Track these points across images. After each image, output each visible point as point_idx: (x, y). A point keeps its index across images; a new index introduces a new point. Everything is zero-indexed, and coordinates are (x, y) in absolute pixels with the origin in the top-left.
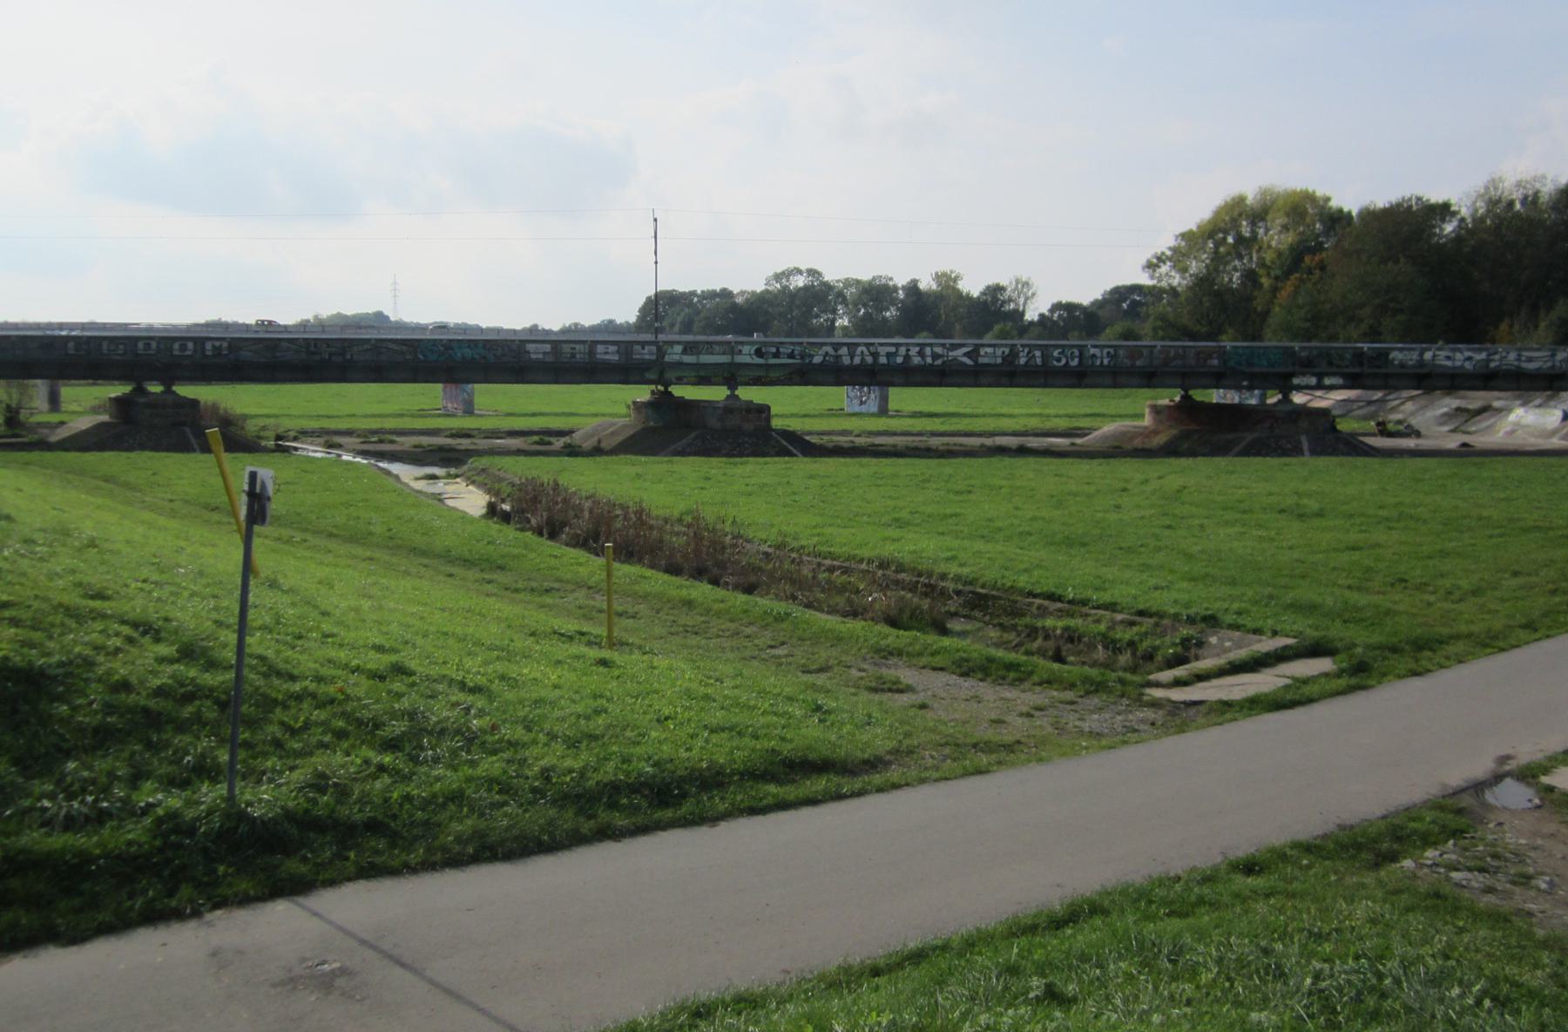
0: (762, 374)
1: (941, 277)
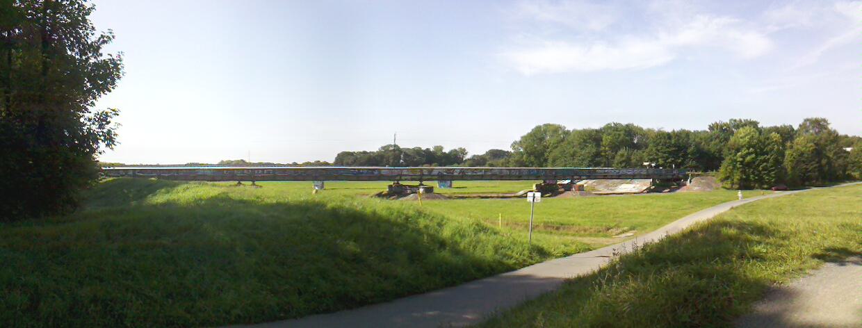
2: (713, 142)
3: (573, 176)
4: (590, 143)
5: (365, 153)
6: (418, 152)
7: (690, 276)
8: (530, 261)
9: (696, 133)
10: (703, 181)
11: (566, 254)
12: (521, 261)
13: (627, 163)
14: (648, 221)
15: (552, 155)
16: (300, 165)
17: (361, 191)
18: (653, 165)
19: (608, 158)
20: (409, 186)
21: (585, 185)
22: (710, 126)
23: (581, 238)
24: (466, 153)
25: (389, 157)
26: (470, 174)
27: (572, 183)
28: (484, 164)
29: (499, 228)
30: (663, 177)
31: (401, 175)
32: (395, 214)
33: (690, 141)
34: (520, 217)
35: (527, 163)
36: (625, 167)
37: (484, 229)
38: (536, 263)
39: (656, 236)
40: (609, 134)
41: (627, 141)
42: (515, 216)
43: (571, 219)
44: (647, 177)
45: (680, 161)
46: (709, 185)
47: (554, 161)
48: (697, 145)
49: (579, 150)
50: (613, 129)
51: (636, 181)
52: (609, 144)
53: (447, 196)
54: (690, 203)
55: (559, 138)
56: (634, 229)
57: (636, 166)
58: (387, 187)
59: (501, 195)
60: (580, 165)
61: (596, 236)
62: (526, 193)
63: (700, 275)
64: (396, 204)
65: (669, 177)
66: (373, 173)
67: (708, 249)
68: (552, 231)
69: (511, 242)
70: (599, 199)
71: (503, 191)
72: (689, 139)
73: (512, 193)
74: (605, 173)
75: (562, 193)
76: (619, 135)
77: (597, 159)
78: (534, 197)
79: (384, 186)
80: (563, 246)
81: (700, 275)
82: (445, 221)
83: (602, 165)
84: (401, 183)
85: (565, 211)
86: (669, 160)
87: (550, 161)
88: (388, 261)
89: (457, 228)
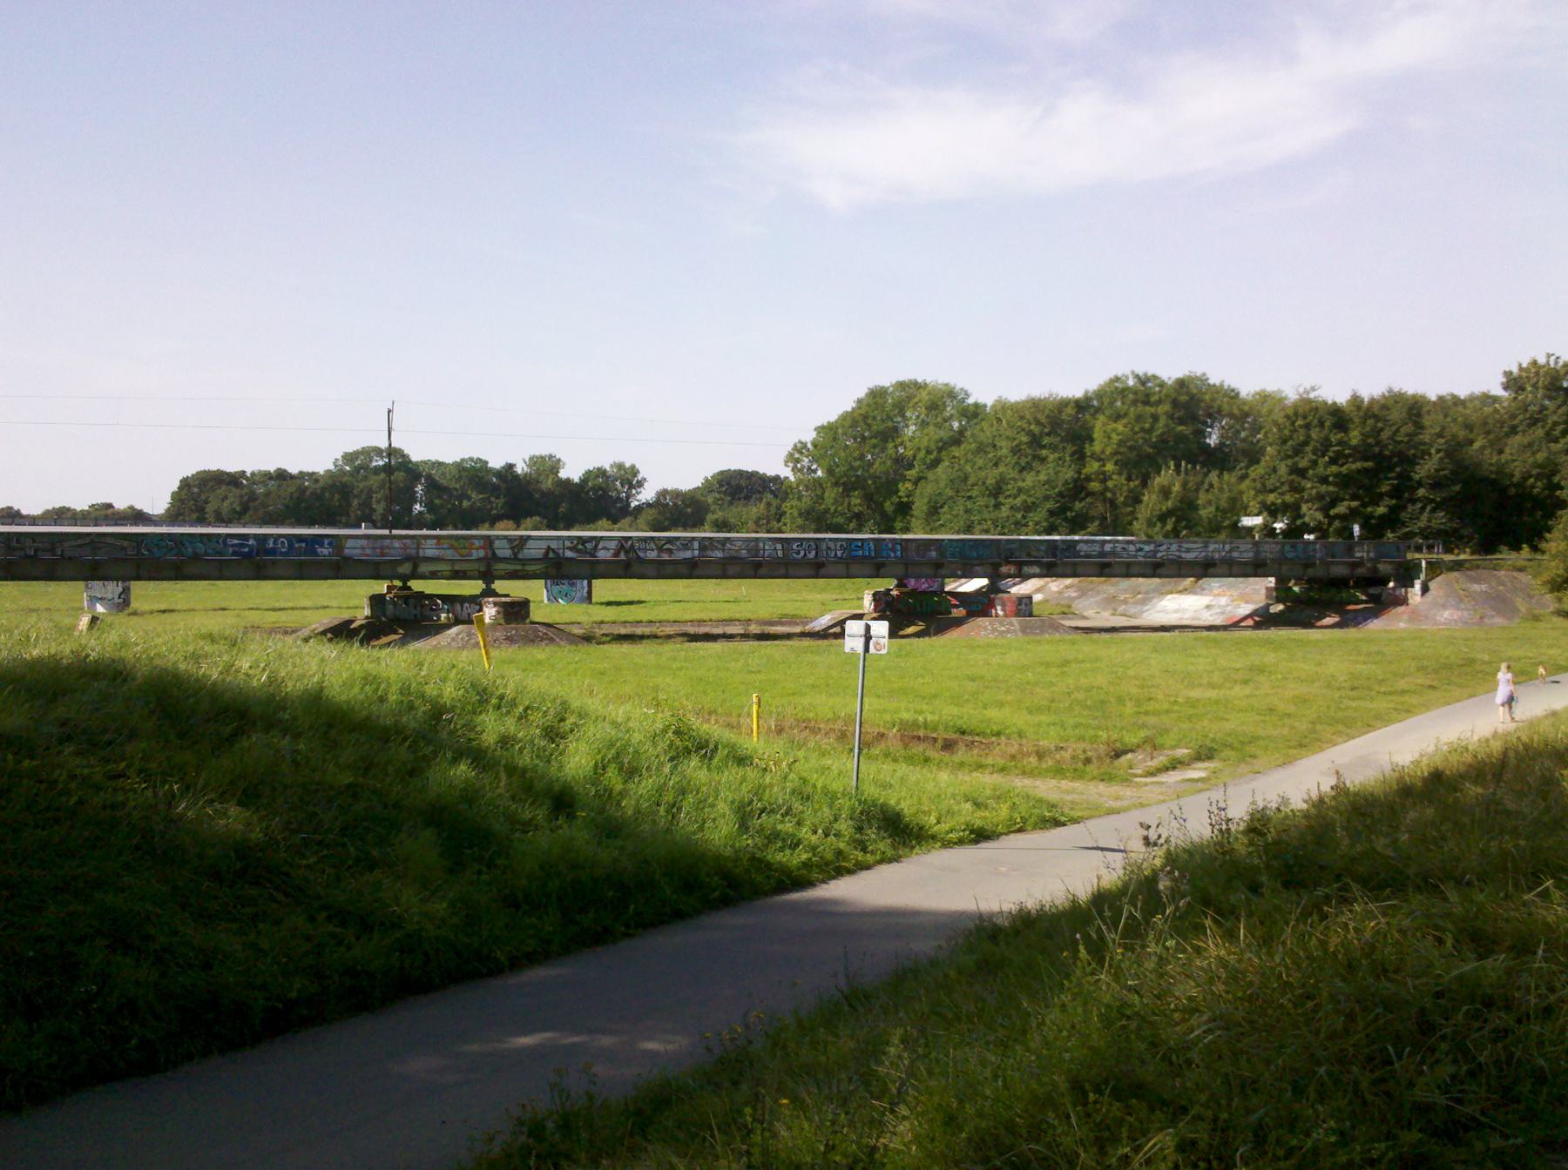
0: (518, 567)
1: (535, 461)
2: (1518, 440)
3: (996, 566)
4: (1053, 447)
5: (282, 475)
6: (474, 475)
7: (1440, 941)
8: (860, 855)
9: (1448, 405)
10: (1476, 587)
11: (980, 836)
12: (829, 856)
13: (1182, 517)
14: (1260, 732)
15: (927, 489)
16: (33, 520)
17: (272, 617)
18: (1278, 526)
19: (1112, 502)
20: (449, 599)
21: (1037, 598)
22: (1508, 374)
23: (1027, 782)
24: (640, 484)
25: (370, 491)
26: (652, 555)
27: (994, 589)
28: (696, 521)
29: (753, 742)
30: (1319, 572)
31: (415, 561)
32: (393, 698)
33: (1426, 437)
34: (822, 705)
35: (840, 520)
36: (1176, 533)
37: (703, 748)
38: (880, 862)
39: (1296, 785)
40: (1118, 417)
41: (1181, 438)
42: (806, 701)
43: (992, 713)
44: (1256, 568)
45: (1381, 510)
46: (1501, 604)
47: (934, 511)
48: (1454, 450)
49: (1013, 474)
50: (1134, 397)
51: (1215, 584)
52: (1116, 453)
53: (577, 631)
54: (1422, 669)
55: (943, 434)
56: (1210, 758)
57: (1214, 528)
58: (366, 602)
59: (754, 629)
60: (1019, 526)
61: (1078, 775)
62: (842, 623)
63: (1480, 941)
64: (395, 664)
65: (1339, 571)
66: (315, 553)
67: (1509, 844)
68: (931, 753)
69: (793, 792)
70: (1087, 647)
71: (764, 613)
72: (1420, 427)
73: (792, 620)
74: (1102, 554)
75: (958, 622)
76: (1155, 418)
77: (1078, 505)
78: (868, 637)
79: (353, 598)
80: (968, 806)
81: (1480, 941)
82: (571, 720)
83: (1093, 527)
84: (417, 585)
85: (971, 686)
86: (1341, 509)
87: (910, 512)
88: (371, 868)
89: (612, 744)
